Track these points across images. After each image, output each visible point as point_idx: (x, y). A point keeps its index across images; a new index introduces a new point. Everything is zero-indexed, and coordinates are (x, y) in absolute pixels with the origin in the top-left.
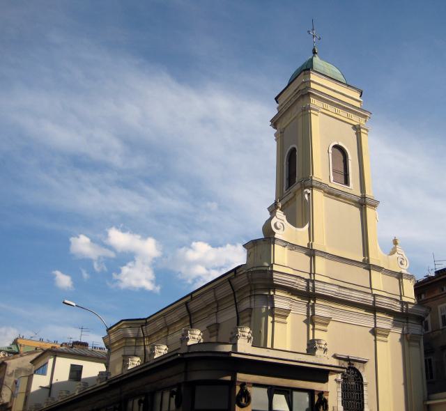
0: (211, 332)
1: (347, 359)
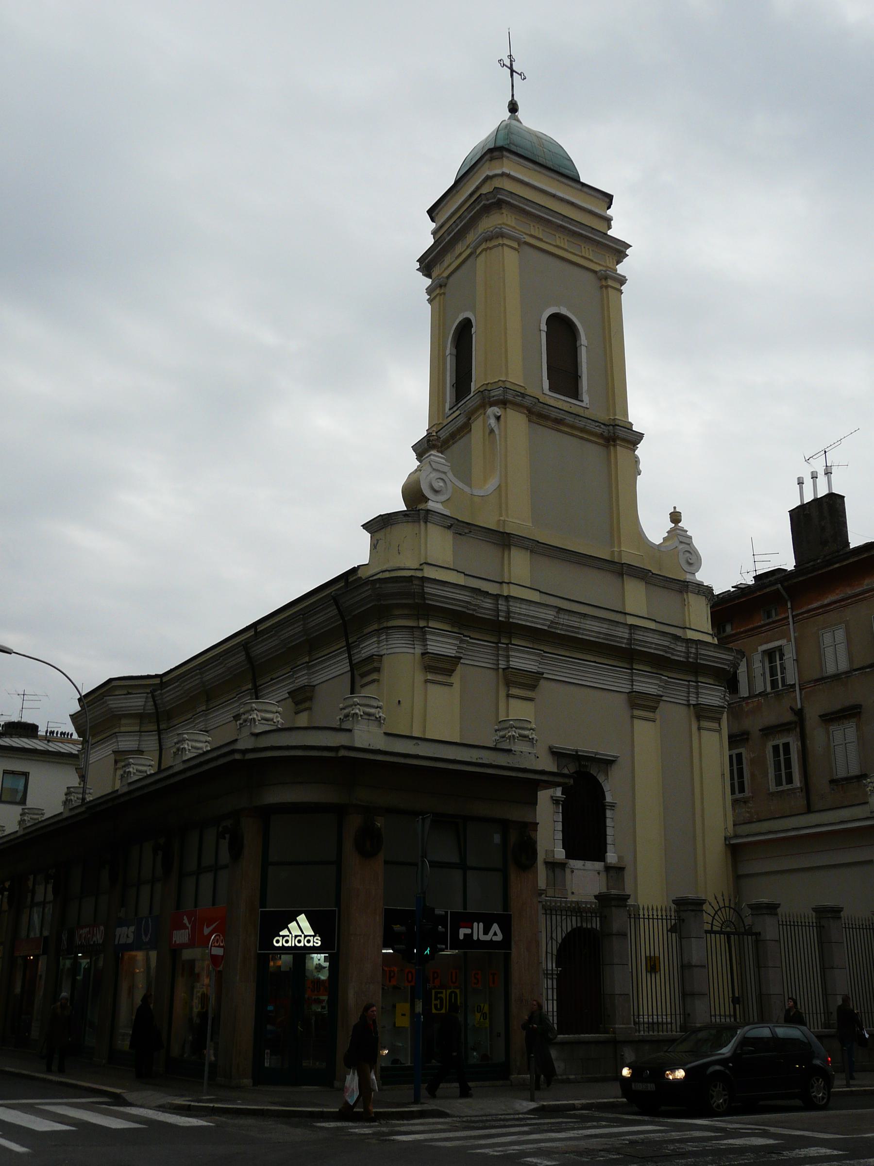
0: (297, 703)
1: (576, 757)
